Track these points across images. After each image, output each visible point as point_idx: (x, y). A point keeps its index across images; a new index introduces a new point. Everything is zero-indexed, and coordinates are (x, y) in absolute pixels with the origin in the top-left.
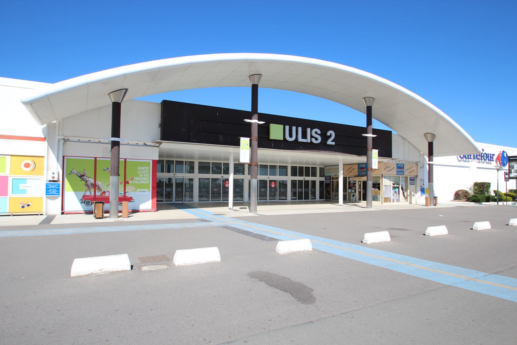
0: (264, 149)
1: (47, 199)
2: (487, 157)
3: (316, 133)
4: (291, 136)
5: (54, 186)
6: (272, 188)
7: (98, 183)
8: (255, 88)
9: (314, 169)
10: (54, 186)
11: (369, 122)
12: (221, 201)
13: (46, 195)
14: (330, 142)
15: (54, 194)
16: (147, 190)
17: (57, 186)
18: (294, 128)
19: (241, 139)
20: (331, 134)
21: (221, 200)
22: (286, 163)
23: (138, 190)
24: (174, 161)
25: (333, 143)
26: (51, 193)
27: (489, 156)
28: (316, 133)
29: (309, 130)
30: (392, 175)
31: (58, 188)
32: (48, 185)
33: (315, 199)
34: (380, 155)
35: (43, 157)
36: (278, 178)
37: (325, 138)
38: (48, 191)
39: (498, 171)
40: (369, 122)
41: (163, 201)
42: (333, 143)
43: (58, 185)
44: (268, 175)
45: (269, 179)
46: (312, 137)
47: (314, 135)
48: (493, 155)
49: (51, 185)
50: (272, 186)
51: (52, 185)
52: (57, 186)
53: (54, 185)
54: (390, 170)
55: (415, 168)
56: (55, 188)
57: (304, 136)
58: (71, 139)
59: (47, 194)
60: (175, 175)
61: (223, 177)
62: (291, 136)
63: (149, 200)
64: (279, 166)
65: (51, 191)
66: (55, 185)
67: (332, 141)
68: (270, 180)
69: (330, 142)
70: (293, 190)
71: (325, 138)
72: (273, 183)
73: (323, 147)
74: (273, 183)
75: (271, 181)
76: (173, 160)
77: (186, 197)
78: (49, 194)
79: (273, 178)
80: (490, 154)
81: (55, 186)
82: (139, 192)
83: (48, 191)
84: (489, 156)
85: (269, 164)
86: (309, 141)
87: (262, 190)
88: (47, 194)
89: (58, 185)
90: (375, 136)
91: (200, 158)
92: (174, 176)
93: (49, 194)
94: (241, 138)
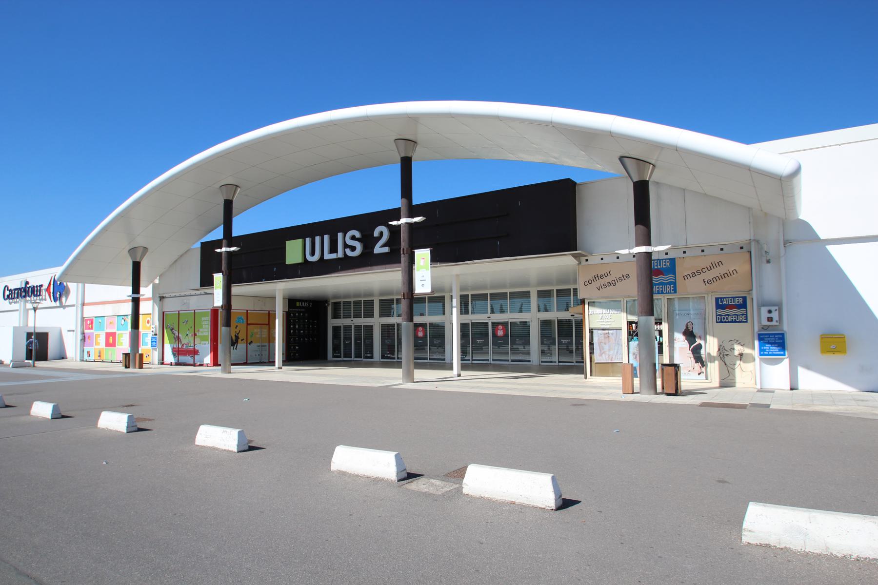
0: (516, 259)
1: (765, 366)
2: (33, 292)
3: (353, 238)
4: (313, 253)
5: (774, 339)
6: (499, 337)
7: (180, 335)
8: (406, 164)
9: (369, 304)
10: (774, 339)
11: (407, 191)
12: (573, 362)
13: (760, 355)
14: (378, 249)
15: (775, 353)
16: (208, 342)
17: (779, 339)
18: (318, 239)
19: (214, 276)
20: (381, 234)
21: (575, 362)
22: (527, 284)
23: (202, 342)
24: (570, 289)
25: (386, 250)
26: (768, 352)
27: (36, 288)
28: (353, 238)
29: (340, 235)
30: (629, 296)
31: (780, 341)
32: (761, 336)
33: (372, 357)
34: (436, 259)
35: (150, 314)
36: (511, 317)
37: (368, 241)
38: (762, 348)
39: (35, 311)
40: (407, 191)
41: (426, 359)
42: (386, 250)
43: (781, 336)
44: (487, 313)
45: (491, 321)
46: (346, 246)
47: (350, 242)
48: (41, 286)
49: (768, 336)
50: (498, 333)
51: (769, 337)
52: (779, 339)
53: (773, 336)
54: (613, 283)
55: (742, 267)
56: (776, 341)
57: (333, 249)
58: (167, 295)
59: (762, 353)
60: (352, 321)
61: (490, 317)
62: (313, 253)
63: (208, 355)
64: (558, 291)
65: (768, 348)
66: (776, 336)
67: (384, 246)
68: (493, 323)
69: (378, 249)
70: (387, 342)
71: (368, 241)
72: (500, 327)
73: (367, 260)
74: (500, 327)
75: (495, 325)
76: (372, 299)
77: (473, 355)
78: (765, 353)
79: (498, 317)
80: (37, 286)
81: (775, 338)
82: (203, 344)
83: (762, 348)
84: (36, 288)
85: (489, 292)
86: (340, 254)
87: (563, 341)
88: (762, 353)
89: (781, 336)
90: (218, 250)
91: (381, 294)
92: (352, 322)
93: (765, 353)
94: (415, 250)
